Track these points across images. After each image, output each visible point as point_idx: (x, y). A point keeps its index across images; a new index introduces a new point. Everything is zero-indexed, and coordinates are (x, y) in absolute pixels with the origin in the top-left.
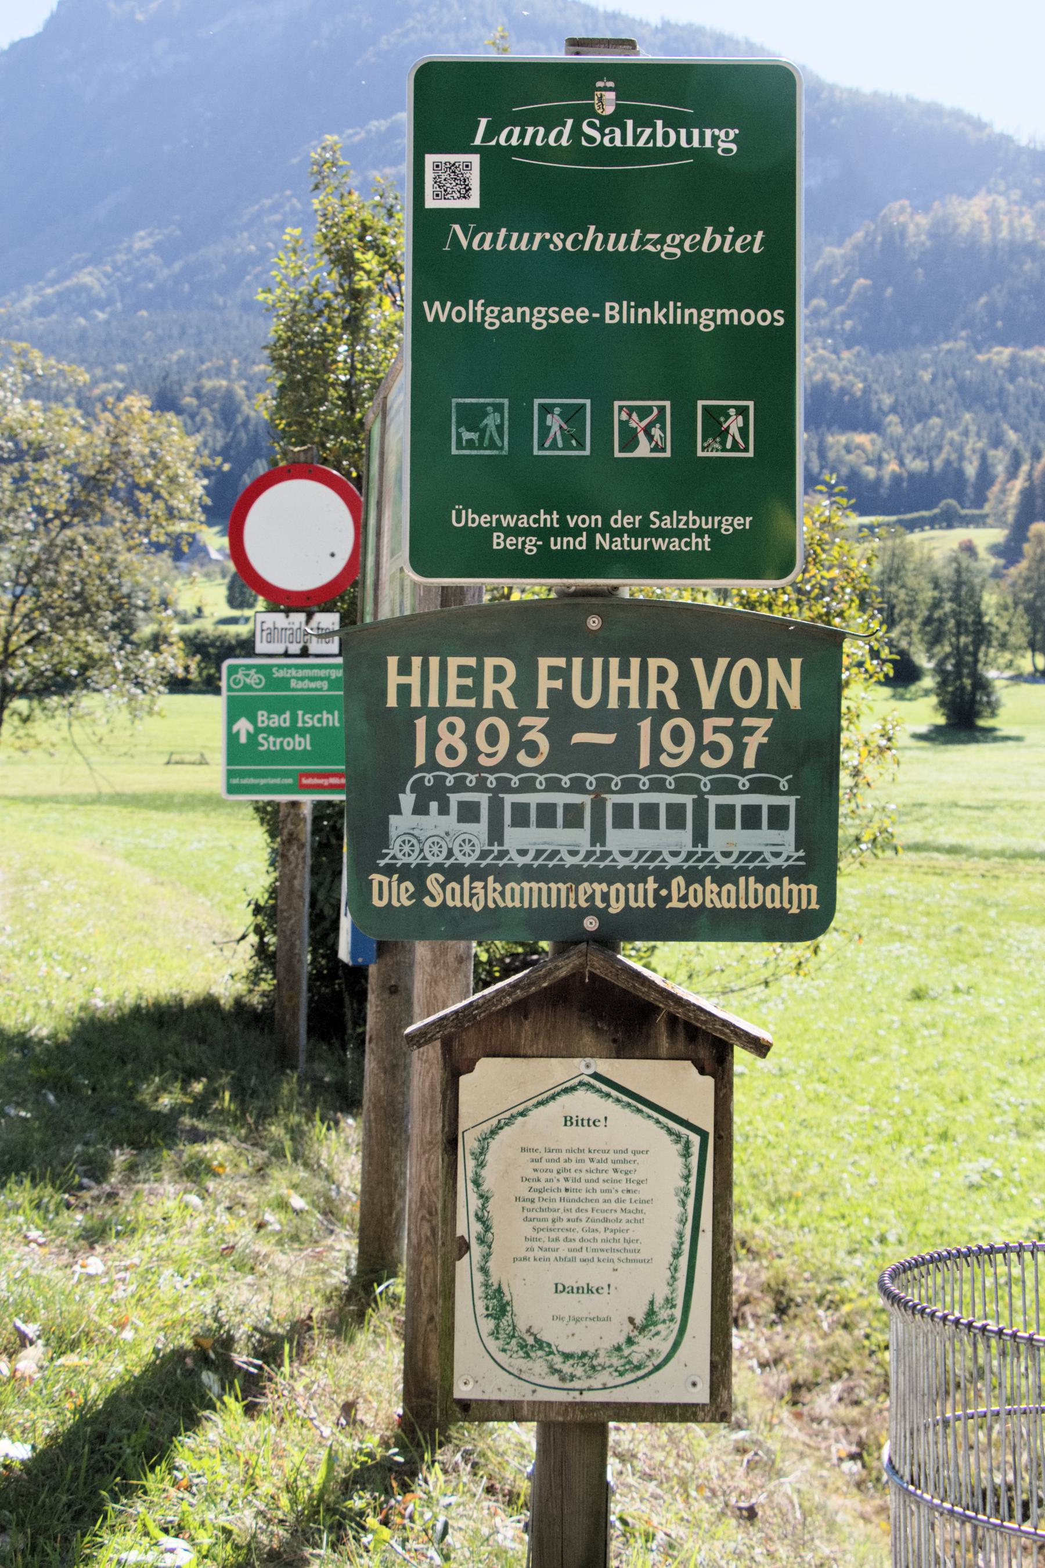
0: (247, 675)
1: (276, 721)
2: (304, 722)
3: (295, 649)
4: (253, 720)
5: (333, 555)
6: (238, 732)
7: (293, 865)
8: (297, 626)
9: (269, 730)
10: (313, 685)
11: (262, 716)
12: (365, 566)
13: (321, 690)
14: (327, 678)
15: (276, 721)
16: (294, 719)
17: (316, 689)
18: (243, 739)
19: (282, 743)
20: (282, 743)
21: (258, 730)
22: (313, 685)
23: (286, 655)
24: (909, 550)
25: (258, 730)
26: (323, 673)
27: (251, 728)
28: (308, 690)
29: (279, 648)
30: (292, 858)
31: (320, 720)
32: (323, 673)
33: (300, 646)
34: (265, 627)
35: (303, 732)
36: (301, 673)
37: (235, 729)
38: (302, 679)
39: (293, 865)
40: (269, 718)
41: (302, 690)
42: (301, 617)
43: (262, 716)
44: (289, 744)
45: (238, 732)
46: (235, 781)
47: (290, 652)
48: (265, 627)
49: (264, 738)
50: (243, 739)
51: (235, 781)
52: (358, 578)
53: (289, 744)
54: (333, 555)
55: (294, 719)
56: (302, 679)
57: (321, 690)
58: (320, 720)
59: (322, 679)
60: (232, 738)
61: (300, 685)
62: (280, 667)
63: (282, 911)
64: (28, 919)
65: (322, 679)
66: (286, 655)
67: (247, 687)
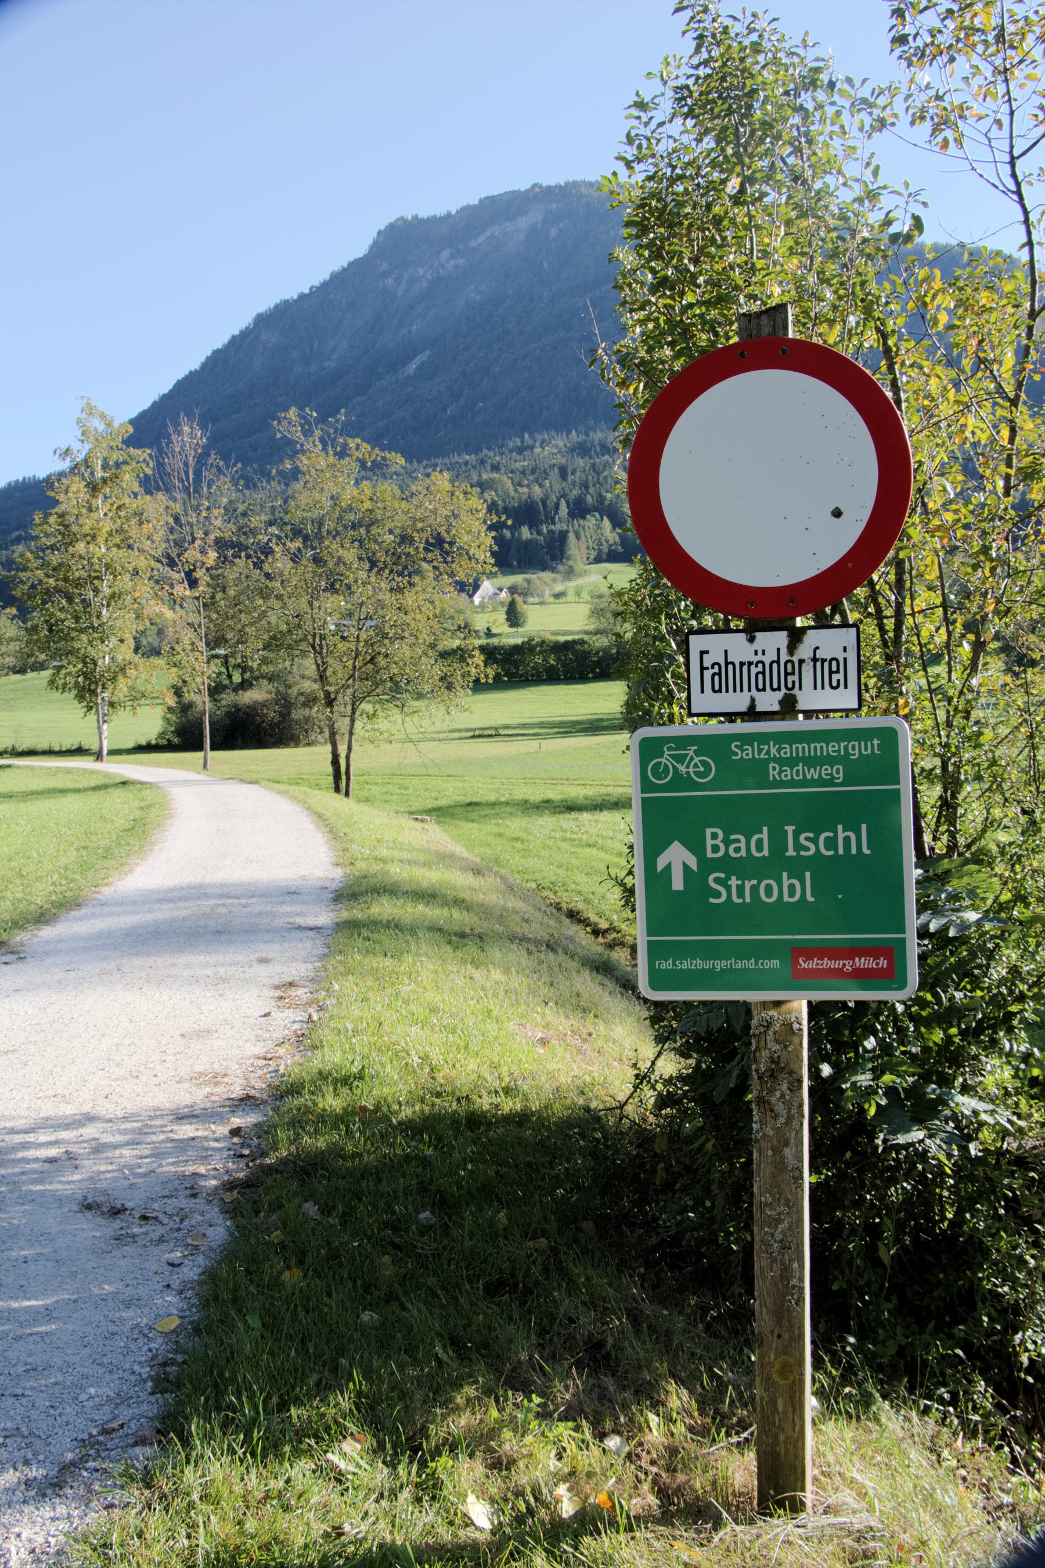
0: (680, 759)
1: (741, 847)
2: (798, 847)
3: (769, 701)
4: (697, 847)
5: (837, 513)
6: (668, 868)
7: (782, 1120)
8: (771, 656)
9: (727, 865)
10: (812, 774)
11: (713, 837)
12: (804, 1458)
13: (830, 783)
14: (843, 759)
15: (741, 847)
16: (778, 843)
17: (821, 782)
18: (678, 883)
19: (755, 889)
20: (755, 889)
21: (707, 866)
22: (812, 774)
23: (752, 714)
24: (922, 245)
25: (707, 866)
26: (832, 749)
27: (693, 862)
28: (804, 783)
29: (738, 702)
30: (779, 1107)
31: (831, 843)
32: (832, 749)
33: (780, 695)
34: (708, 661)
35: (796, 870)
36: (787, 751)
37: (661, 863)
38: (792, 762)
39: (782, 1120)
40: (727, 842)
41: (792, 783)
42: (780, 639)
43: (713, 837)
44: (769, 890)
45: (668, 868)
46: (666, 965)
47: (760, 708)
48: (708, 661)
49: (717, 880)
50: (678, 883)
51: (666, 965)
52: (794, 1282)
53: (769, 890)
54: (837, 513)
55: (778, 843)
56: (792, 762)
57: (830, 783)
58: (831, 843)
59: (830, 761)
60: (657, 879)
61: (788, 774)
62: (746, 739)
63: (762, 1206)
64: (291, 1277)
65: (830, 761)
66: (752, 714)
67: (681, 782)
